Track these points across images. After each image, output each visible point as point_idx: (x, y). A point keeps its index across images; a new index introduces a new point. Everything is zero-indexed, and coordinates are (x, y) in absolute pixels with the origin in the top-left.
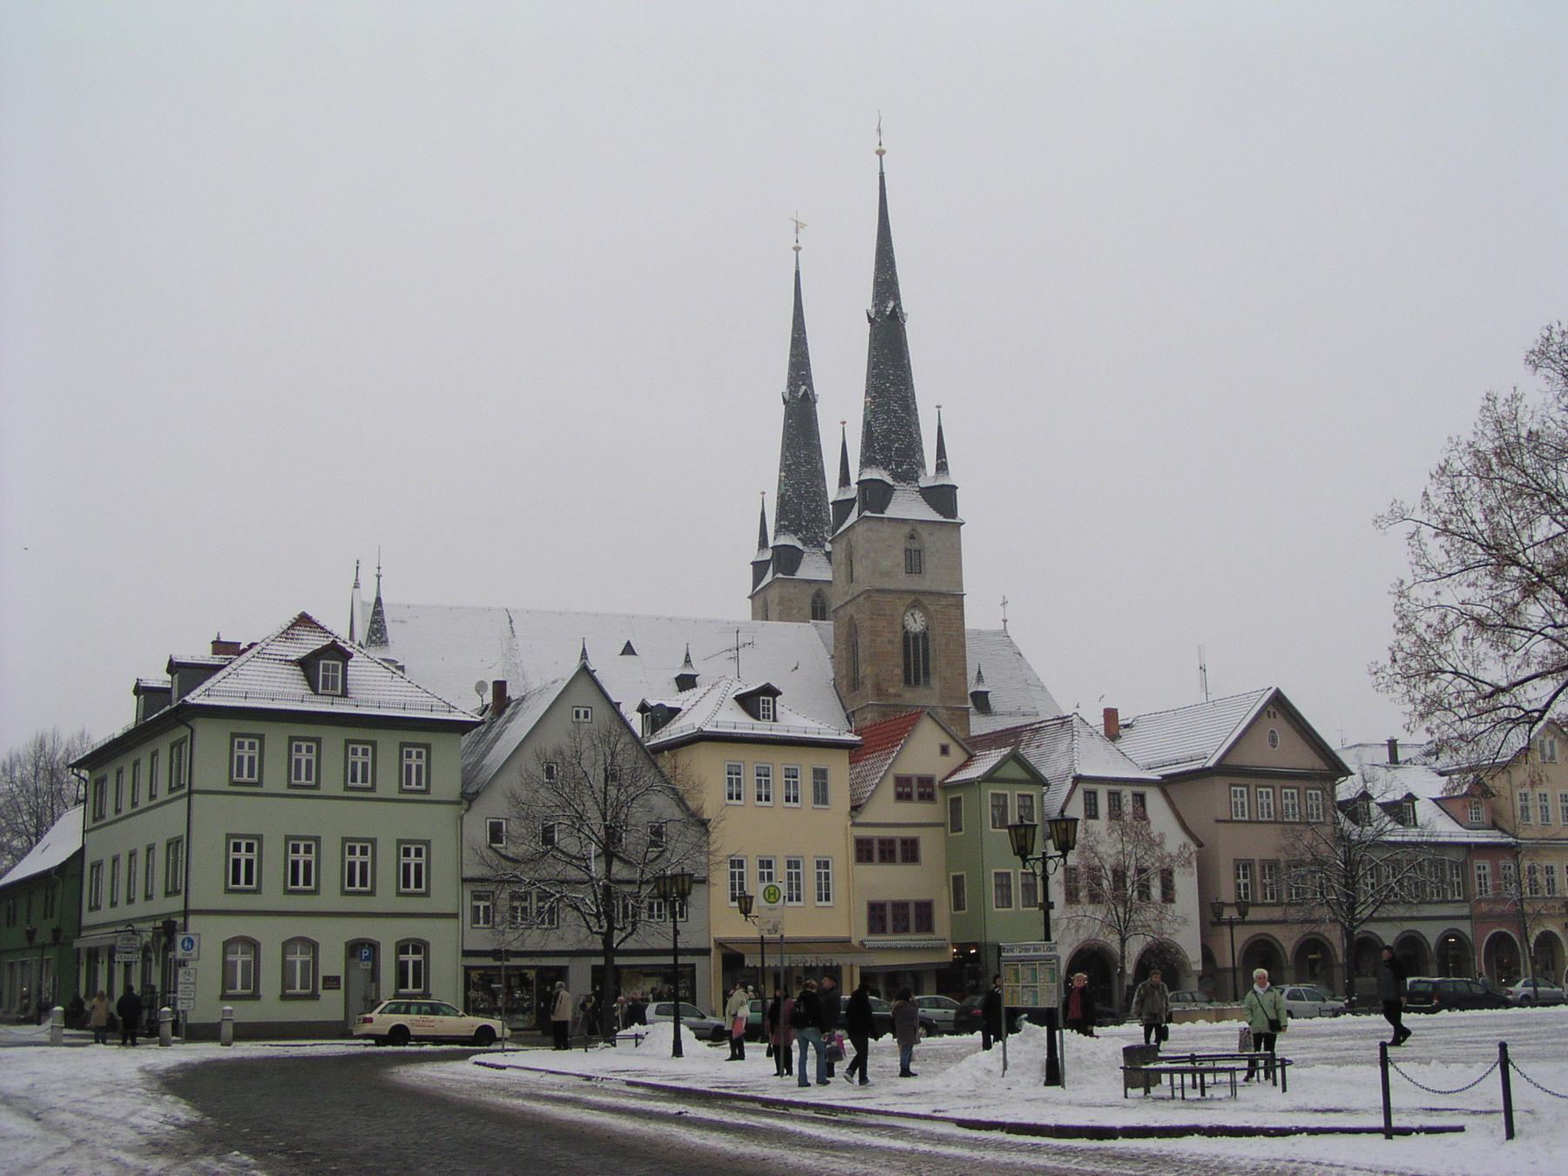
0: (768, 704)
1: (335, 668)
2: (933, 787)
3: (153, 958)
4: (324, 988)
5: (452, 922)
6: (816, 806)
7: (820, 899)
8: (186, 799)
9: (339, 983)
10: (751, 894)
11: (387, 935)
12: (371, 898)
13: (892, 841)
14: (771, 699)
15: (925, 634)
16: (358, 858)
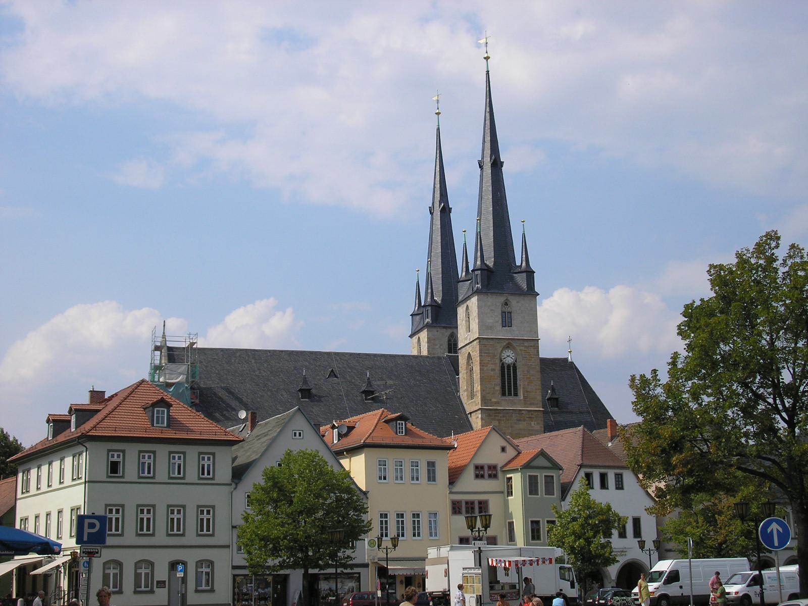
0: (402, 425)
1: (163, 412)
2: (497, 471)
3: (62, 572)
4: (157, 587)
5: (226, 550)
6: (429, 483)
7: (431, 535)
8: (84, 485)
9: (165, 585)
10: (644, 540)
11: (192, 557)
12: (183, 538)
13: (472, 503)
14: (404, 422)
15: (514, 364)
16: (145, 516)
